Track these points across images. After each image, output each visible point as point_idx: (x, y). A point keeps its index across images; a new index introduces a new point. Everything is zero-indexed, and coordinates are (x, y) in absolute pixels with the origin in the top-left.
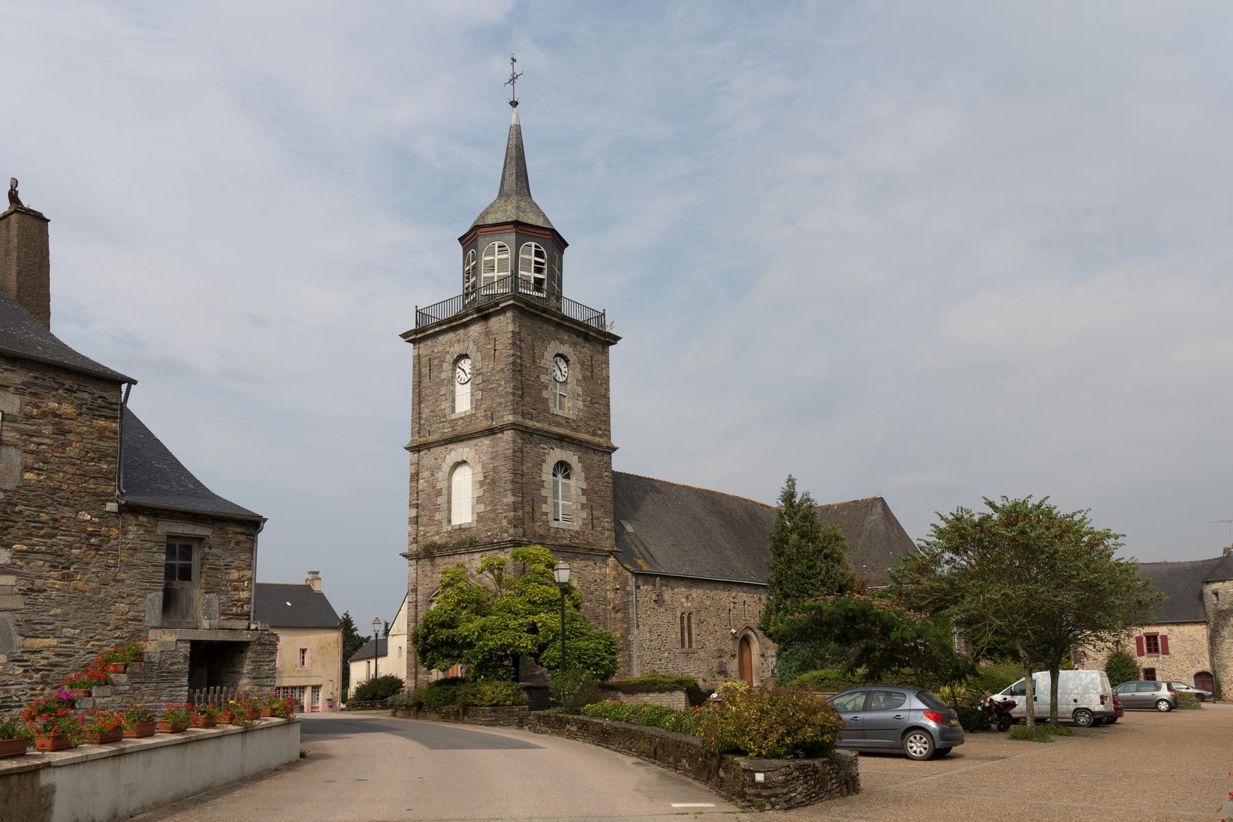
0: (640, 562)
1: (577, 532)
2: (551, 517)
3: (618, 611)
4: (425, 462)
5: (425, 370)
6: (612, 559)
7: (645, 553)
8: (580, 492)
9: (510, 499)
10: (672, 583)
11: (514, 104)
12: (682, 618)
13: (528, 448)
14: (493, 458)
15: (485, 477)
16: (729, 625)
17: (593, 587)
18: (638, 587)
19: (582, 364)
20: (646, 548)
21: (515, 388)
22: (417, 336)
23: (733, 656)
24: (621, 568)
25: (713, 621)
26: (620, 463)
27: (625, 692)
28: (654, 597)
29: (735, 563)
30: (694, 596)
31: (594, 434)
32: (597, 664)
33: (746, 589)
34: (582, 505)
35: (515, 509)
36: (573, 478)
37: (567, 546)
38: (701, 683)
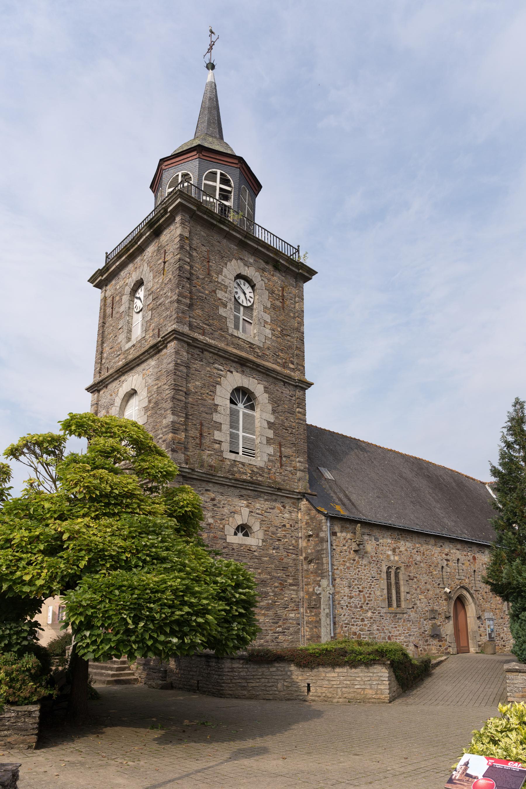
0: (338, 508)
1: (261, 468)
2: (226, 447)
3: (310, 562)
4: (103, 401)
5: (109, 311)
6: (305, 502)
7: (345, 500)
8: (266, 425)
9: (171, 418)
10: (376, 532)
11: (211, 66)
12: (388, 573)
13: (197, 365)
14: (157, 379)
15: (150, 402)
16: (441, 585)
17: (280, 533)
18: (334, 534)
19: (272, 292)
20: (346, 496)
21: (180, 295)
22: (102, 279)
23: (448, 618)
24: (314, 512)
25: (424, 578)
26: (322, 411)
27: (299, 665)
28: (354, 546)
29: (446, 521)
30: (402, 549)
31: (284, 366)
32: (182, 622)
33: (459, 546)
34: (269, 440)
35: (175, 430)
36: (258, 409)
37: (245, 481)
38: (411, 651)
